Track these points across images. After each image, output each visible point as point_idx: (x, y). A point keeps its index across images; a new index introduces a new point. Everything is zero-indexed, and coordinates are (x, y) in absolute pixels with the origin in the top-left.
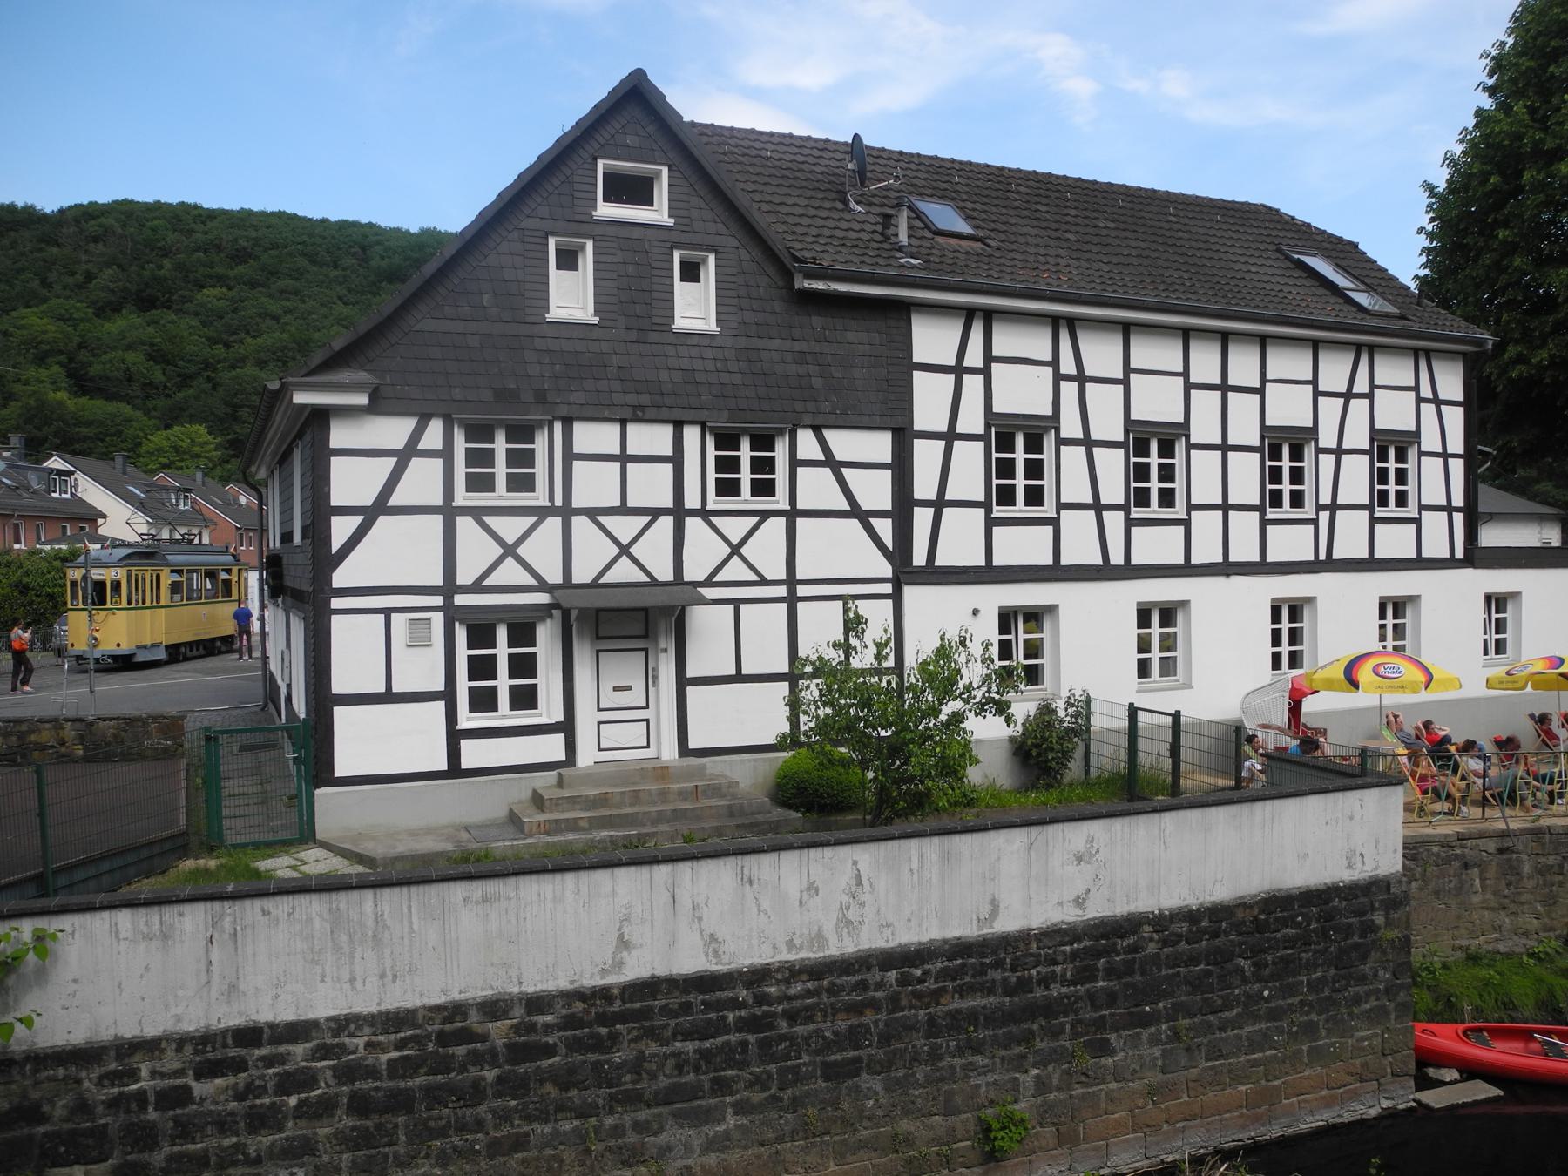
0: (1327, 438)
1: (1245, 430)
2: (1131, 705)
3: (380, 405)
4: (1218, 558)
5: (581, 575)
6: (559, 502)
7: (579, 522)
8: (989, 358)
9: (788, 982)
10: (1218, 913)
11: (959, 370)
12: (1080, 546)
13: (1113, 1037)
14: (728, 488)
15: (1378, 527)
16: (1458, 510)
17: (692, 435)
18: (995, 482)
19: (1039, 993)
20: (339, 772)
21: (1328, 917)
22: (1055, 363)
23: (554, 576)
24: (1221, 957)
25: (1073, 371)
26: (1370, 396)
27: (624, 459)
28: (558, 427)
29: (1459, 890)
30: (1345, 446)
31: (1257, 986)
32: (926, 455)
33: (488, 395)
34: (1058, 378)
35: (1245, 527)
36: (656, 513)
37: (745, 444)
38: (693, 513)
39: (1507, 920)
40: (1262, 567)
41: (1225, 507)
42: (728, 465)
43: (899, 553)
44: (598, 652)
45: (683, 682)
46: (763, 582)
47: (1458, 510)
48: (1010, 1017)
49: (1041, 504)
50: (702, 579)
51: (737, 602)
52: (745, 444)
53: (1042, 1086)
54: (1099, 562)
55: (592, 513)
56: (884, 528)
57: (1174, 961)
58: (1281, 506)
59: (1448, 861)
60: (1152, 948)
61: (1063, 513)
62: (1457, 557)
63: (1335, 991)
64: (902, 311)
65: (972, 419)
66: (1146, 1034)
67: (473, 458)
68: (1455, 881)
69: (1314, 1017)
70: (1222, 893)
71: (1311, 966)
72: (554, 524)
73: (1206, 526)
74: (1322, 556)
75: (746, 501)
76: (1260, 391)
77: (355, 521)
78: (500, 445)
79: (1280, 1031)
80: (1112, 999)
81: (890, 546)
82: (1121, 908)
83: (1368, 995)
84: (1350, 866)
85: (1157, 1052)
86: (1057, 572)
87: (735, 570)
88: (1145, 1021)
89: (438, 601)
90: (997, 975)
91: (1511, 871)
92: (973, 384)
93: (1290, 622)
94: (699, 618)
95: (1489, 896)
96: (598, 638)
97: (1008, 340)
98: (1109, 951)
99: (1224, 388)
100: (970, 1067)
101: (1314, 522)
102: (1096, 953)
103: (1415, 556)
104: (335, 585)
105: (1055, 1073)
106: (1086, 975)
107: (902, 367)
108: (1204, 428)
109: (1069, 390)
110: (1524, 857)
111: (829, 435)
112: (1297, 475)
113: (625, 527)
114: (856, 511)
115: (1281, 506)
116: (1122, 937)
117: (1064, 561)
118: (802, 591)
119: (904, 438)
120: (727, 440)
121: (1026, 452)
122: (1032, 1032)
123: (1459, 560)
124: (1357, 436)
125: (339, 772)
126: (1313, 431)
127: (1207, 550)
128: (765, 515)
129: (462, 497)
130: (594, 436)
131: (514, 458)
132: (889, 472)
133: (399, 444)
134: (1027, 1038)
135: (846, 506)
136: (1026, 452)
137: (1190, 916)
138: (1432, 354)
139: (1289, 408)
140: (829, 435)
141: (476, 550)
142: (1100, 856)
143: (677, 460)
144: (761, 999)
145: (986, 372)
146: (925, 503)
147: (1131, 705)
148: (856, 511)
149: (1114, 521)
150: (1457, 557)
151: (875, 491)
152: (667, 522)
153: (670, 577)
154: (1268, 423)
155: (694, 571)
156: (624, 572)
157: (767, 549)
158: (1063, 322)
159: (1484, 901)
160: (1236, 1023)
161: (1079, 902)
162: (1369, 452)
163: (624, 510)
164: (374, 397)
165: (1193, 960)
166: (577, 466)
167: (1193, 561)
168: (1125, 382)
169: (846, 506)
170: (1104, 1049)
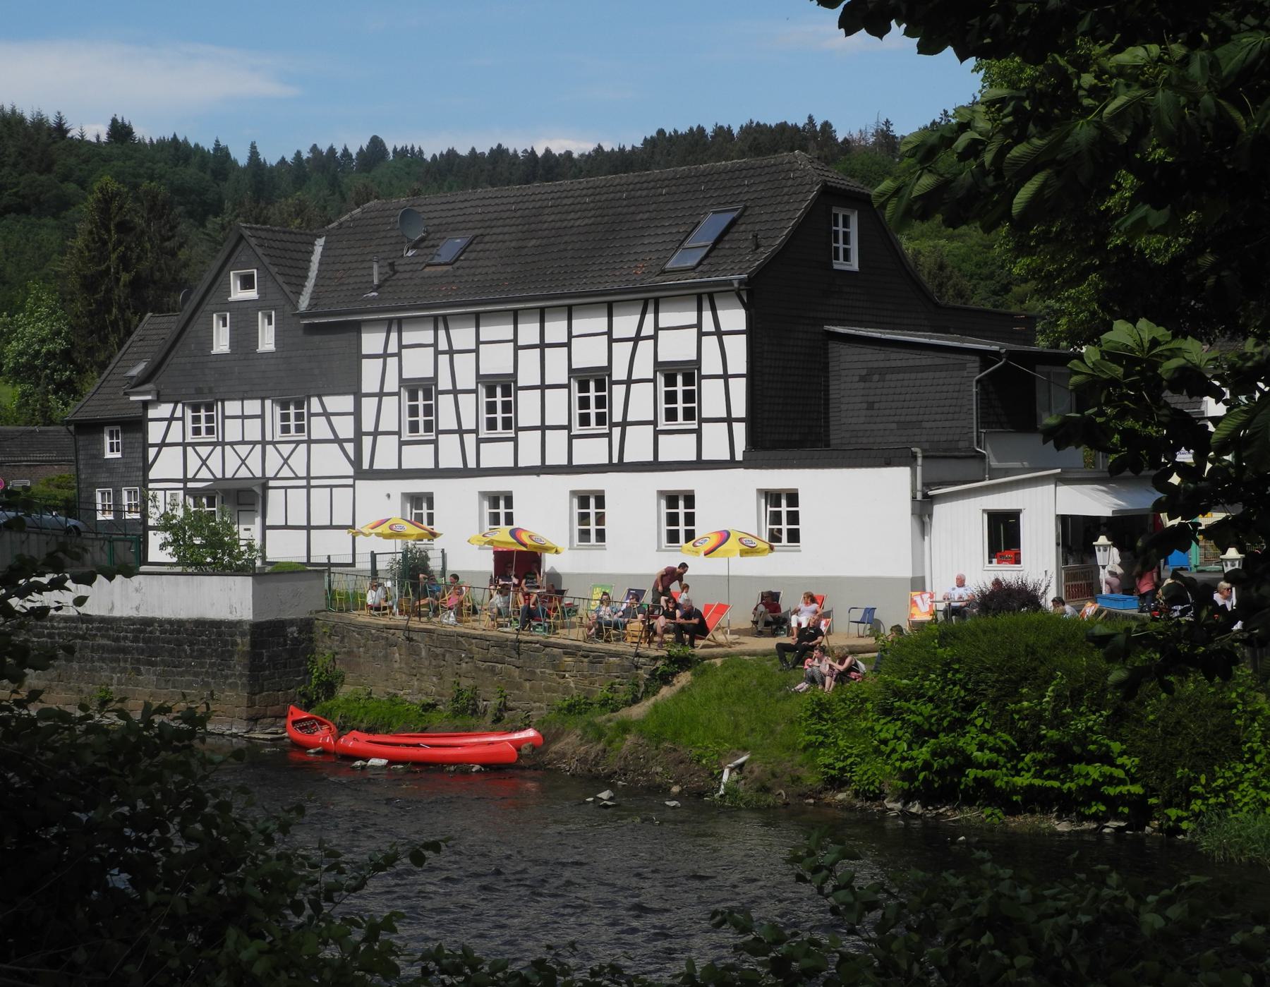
2: (372, 552)
4: (649, 457)
5: (229, 475)
7: (228, 448)
8: (401, 347)
9: (59, 622)
10: (180, 623)
11: (385, 356)
13: (142, 668)
14: (285, 429)
15: (661, 437)
16: (739, 420)
17: (268, 403)
19: (122, 643)
20: (150, 560)
21: (220, 634)
22: (435, 345)
23: (219, 476)
24: (179, 644)
25: (446, 348)
26: (655, 337)
28: (219, 404)
29: (386, 657)
32: (369, 405)
33: (193, 391)
34: (437, 353)
35: (557, 441)
36: (254, 443)
37: (292, 407)
38: (269, 443)
40: (570, 469)
42: (285, 417)
43: (356, 462)
45: (265, 528)
46: (297, 478)
47: (739, 420)
48: (113, 651)
51: (286, 488)
52: (292, 407)
54: (461, 466)
55: (232, 444)
56: (350, 447)
57: (164, 641)
59: (377, 638)
61: (440, 436)
64: (356, 328)
65: (392, 384)
68: (384, 652)
69: (210, 680)
70: (183, 615)
71: (211, 656)
72: (219, 449)
73: (449, 445)
74: (615, 460)
76: (568, 345)
77: (156, 449)
80: (142, 652)
81: (352, 458)
82: (150, 615)
83: (232, 675)
84: (231, 613)
85: (155, 678)
86: (437, 473)
87: (286, 472)
88: (153, 664)
89: (181, 485)
90: (111, 633)
94: (275, 498)
95: (403, 665)
96: (239, 504)
97: (410, 337)
98: (143, 631)
99: (542, 346)
100: (101, 668)
101: (609, 435)
104: (150, 478)
106: (136, 640)
108: (528, 375)
109: (444, 359)
110: (422, 645)
112: (600, 402)
113: (243, 450)
117: (661, 459)
118: (313, 482)
119: (358, 396)
120: (285, 406)
124: (644, 368)
125: (150, 560)
126: (608, 369)
127: (529, 457)
128: (298, 443)
129: (190, 438)
130: (232, 407)
134: (118, 660)
135: (332, 437)
138: (715, 295)
139: (590, 354)
140: (325, 399)
141: (194, 462)
143: (262, 417)
144: (53, 627)
145: (399, 355)
147: (372, 552)
149: (470, 440)
151: (345, 428)
152: (259, 447)
154: (660, 359)
155: (270, 473)
156: (244, 473)
158: (440, 318)
160: (181, 674)
161: (137, 609)
162: (701, 377)
163: (243, 442)
164: (158, 395)
165: (169, 642)
166: (227, 421)
167: (626, 460)
168: (477, 351)
169: (332, 437)
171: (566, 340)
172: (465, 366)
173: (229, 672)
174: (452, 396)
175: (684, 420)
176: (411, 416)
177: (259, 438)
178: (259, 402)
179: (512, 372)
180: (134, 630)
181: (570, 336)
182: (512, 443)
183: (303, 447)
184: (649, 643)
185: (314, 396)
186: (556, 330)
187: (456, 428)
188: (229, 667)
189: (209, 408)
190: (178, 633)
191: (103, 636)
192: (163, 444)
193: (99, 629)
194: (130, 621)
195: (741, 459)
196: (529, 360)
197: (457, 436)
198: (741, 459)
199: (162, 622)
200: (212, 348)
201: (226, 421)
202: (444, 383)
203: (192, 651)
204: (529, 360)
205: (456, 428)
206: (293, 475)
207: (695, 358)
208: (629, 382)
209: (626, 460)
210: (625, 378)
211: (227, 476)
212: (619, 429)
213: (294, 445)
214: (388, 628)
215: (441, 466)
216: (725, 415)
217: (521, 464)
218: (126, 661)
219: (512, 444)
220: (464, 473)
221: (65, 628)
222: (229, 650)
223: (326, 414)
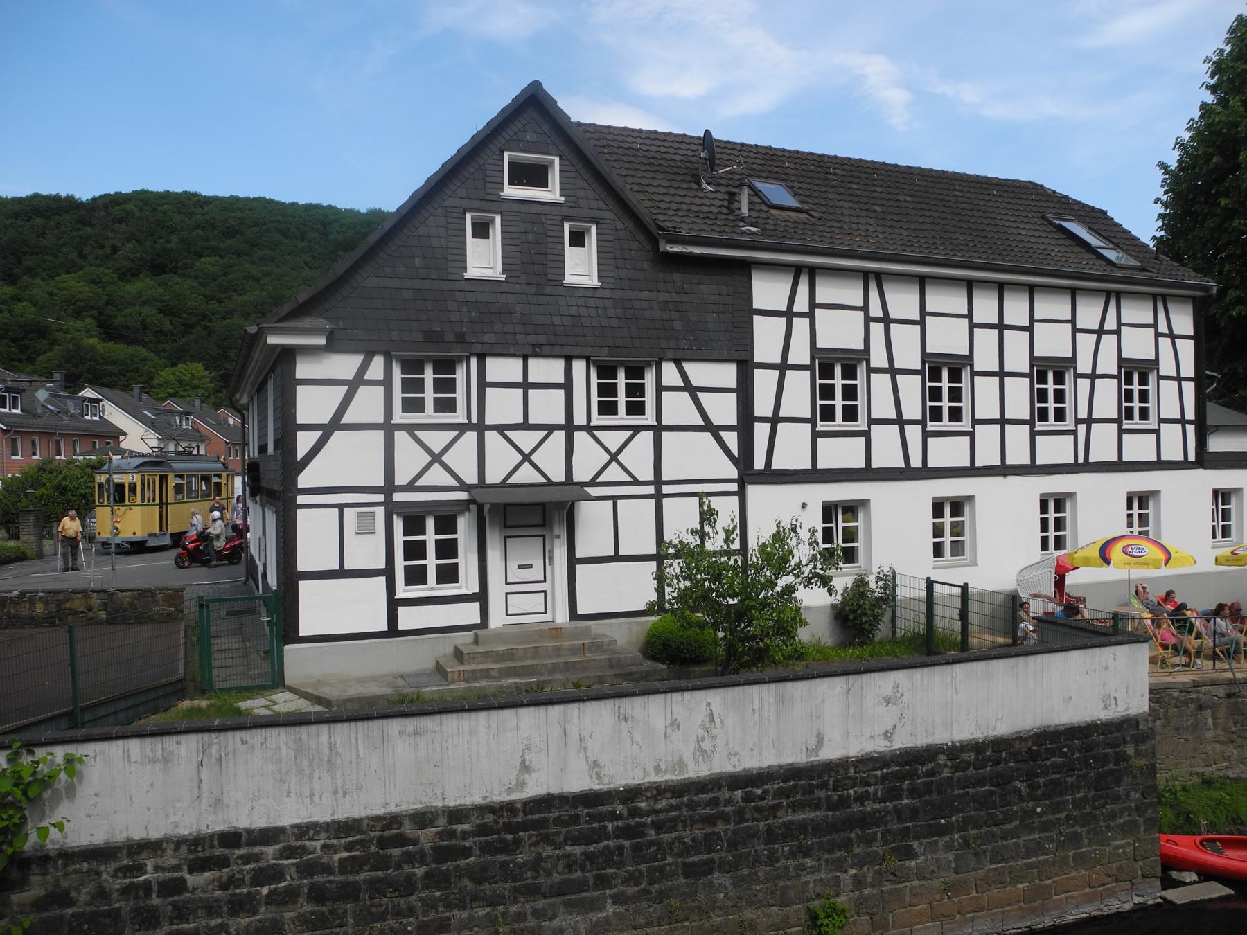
1: (1018, 360)
2: (928, 579)
5: (492, 477)
6: (474, 420)
7: (491, 436)
8: (813, 305)
10: (999, 745)
12: (887, 453)
13: (915, 844)
14: (608, 408)
15: (1125, 437)
16: (1190, 422)
17: (579, 367)
19: (856, 808)
20: (303, 632)
22: (865, 308)
24: (1002, 781)
25: (880, 315)
26: (1117, 332)
28: (474, 361)
29: (1195, 726)
31: (1031, 804)
32: (764, 382)
33: (419, 337)
34: (868, 320)
35: (1018, 436)
36: (551, 428)
37: (621, 375)
38: (580, 428)
41: (1002, 422)
42: (607, 390)
43: (743, 459)
44: (506, 537)
45: (573, 562)
46: (636, 482)
47: (1190, 422)
48: (833, 827)
50: (587, 479)
51: (615, 499)
52: (621, 375)
55: (501, 429)
56: (731, 439)
57: (964, 784)
58: (1047, 421)
59: (1186, 703)
60: (946, 773)
62: (1189, 460)
64: (743, 269)
66: (942, 842)
67: (408, 386)
69: (1078, 829)
70: (1003, 729)
71: (1075, 788)
72: (471, 437)
73: (987, 436)
74: (1081, 460)
75: (622, 419)
79: (1051, 840)
80: (914, 813)
81: (735, 452)
82: (921, 741)
83: (1122, 811)
84: (1105, 707)
85: (951, 856)
86: (868, 474)
87: (614, 473)
89: (380, 498)
92: (801, 325)
94: (586, 511)
96: (506, 526)
97: (827, 291)
98: (912, 775)
99: (1001, 327)
100: (800, 868)
101: (1074, 433)
102: (901, 777)
107: (746, 312)
108: (985, 359)
109: (877, 329)
113: (526, 440)
114: (709, 426)
115: (1047, 421)
116: (923, 764)
118: (666, 489)
122: (850, 840)
124: (1108, 364)
125: (303, 632)
126: (1072, 360)
127: (988, 456)
128: (637, 429)
129: (399, 417)
130: (502, 368)
133: (716, 421)
137: (976, 747)
138: (1167, 298)
139: (1053, 343)
142: (905, 699)
143: (567, 386)
144: (634, 812)
146: (763, 420)
147: (928, 579)
148: (709, 426)
149: (914, 433)
150: (1189, 460)
151: (724, 410)
152: (559, 436)
153: (475, 481)
155: (582, 474)
156: (526, 475)
157: (639, 456)
160: (1015, 834)
161: (888, 735)
162: (1118, 377)
163: (525, 426)
165: (979, 782)
166: (489, 391)
167: (1091, 460)
171: (1027, 324)
172: (1016, 345)
173: (1116, 807)
174: (997, 379)
175: (844, 420)
176: (1063, 391)
177: (561, 420)
178: (520, 362)
179: (967, 353)
180: (884, 778)
181: (1032, 320)
182: (863, 439)
183: (647, 438)
184: (243, 641)
185: (579, 357)
186: (1016, 310)
187: (1179, 417)
188: (1117, 799)
189: (443, 366)
190: (997, 762)
191: (794, 807)
192: (335, 424)
193: (780, 793)
194: (869, 762)
195: (1194, 460)
196: (986, 341)
197: (1179, 426)
198: (1194, 460)
199: (954, 752)
200: (465, 269)
201: (489, 391)
202: (878, 358)
203: (1032, 787)
204: (1086, 343)
205: (1179, 417)
206: (629, 479)
207: (1153, 358)
208: (1093, 377)
209: (1091, 460)
210: (888, 376)
211: (489, 481)
212: (1084, 426)
213: (629, 433)
214: (1196, 685)
215: (1125, 459)
216: (998, 417)
217: (875, 464)
218: (869, 841)
219: (967, 439)
220: (905, 474)
221: (672, 808)
222: (1111, 772)
223: (688, 387)
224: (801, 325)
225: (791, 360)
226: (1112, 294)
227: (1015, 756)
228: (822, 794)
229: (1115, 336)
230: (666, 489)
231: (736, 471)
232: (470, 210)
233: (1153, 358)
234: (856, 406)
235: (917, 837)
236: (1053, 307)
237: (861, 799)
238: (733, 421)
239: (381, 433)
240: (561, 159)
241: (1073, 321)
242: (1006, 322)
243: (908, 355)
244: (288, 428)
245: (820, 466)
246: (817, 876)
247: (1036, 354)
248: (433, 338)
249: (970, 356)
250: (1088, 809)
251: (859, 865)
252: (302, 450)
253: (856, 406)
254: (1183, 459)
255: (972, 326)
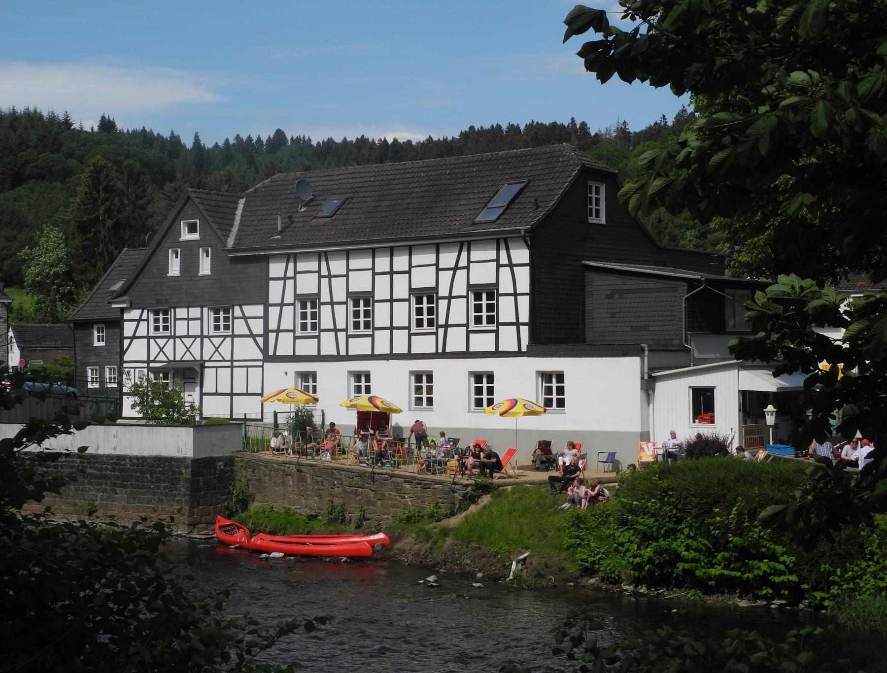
0: (443, 291)
1: (401, 291)
2: (275, 411)
3: (132, 307)
5: (178, 358)
6: (173, 334)
7: (178, 340)
8: (296, 272)
10: (144, 459)
11: (285, 278)
12: (328, 348)
13: (117, 489)
14: (217, 328)
15: (471, 335)
17: (205, 310)
18: (495, 314)
19: (104, 472)
21: (170, 467)
22: (319, 271)
26: (467, 268)
27: (188, 319)
28: (172, 310)
30: (279, 308)
31: (150, 484)
32: (274, 312)
33: (155, 301)
34: (320, 277)
35: (401, 337)
36: (196, 337)
37: (221, 313)
38: (206, 337)
39: (303, 501)
41: (391, 328)
42: (217, 320)
43: (265, 350)
44: (184, 383)
46: (224, 360)
49: (475, 323)
50: (208, 359)
51: (217, 367)
52: (221, 313)
53: (102, 497)
55: (180, 337)
56: (260, 340)
58: (220, 330)
59: (278, 470)
60: (128, 466)
62: (522, 351)
63: (170, 491)
64: (266, 260)
65: (289, 298)
66: (124, 490)
68: (282, 480)
69: (164, 498)
70: (146, 453)
71: (164, 481)
72: (172, 340)
73: (382, 338)
74: (440, 350)
76: (409, 272)
78: (222, 315)
79: (155, 500)
80: (117, 478)
82: (123, 453)
83: (178, 494)
85: (126, 496)
87: (217, 357)
89: (145, 365)
91: (302, 480)
92: (290, 283)
93: (366, 382)
94: (209, 374)
95: (295, 489)
96: (184, 378)
99: (392, 273)
101: (436, 334)
102: (117, 464)
103: (517, 350)
105: (105, 495)
106: (113, 470)
107: (267, 279)
109: (325, 281)
110: (308, 475)
111: (244, 307)
112: (430, 311)
113: (189, 342)
114: (252, 335)
115: (220, 330)
116: (123, 461)
118: (235, 364)
119: (267, 305)
120: (217, 312)
121: (487, 300)
122: (102, 483)
123: (524, 352)
124: (460, 288)
126: (436, 289)
127: (382, 348)
130: (181, 312)
131: (166, 320)
132: (262, 320)
136: (487, 300)
137: (137, 458)
139: (424, 278)
140: (244, 307)
142: (119, 436)
143: (201, 319)
145: (294, 278)
146: (273, 331)
147: (275, 411)
148: (252, 335)
149: (342, 336)
150: (522, 351)
151: (257, 327)
152: (199, 340)
153: (173, 359)
156: (188, 357)
157: (225, 350)
159: (293, 491)
160: (144, 494)
161: (115, 449)
162: (499, 295)
163: (188, 336)
165: (136, 472)
168: (347, 276)
170: (115, 492)
172: (401, 281)
177: (199, 334)
181: (410, 266)
182: (370, 338)
183: (229, 340)
185: (236, 305)
188: (176, 489)
190: (142, 466)
192: (134, 337)
194: (110, 457)
196: (383, 282)
198: (526, 351)
199: (131, 458)
203: (152, 478)
204: (445, 277)
206: (222, 359)
208: (450, 298)
211: (176, 359)
218: (106, 484)
220: (337, 358)
222: (177, 478)
224: (290, 283)
225: (275, 334)
226: (465, 243)
227: (148, 464)
228: (97, 465)
229: (407, 275)
230: (235, 364)
231: (262, 356)
232: (170, 248)
233: (495, 282)
234: (301, 320)
235: (118, 487)
236: (426, 258)
237: (106, 469)
238: (261, 332)
239: (235, 339)
240: (200, 220)
241: (373, 269)
242: (332, 274)
243: (340, 295)
244: (122, 338)
245: (322, 353)
246: (93, 493)
247: (350, 290)
248: (159, 302)
249: (373, 292)
250: (167, 491)
251: (103, 492)
252: (125, 347)
253: (475, 312)
254: (517, 350)
255: (374, 274)
